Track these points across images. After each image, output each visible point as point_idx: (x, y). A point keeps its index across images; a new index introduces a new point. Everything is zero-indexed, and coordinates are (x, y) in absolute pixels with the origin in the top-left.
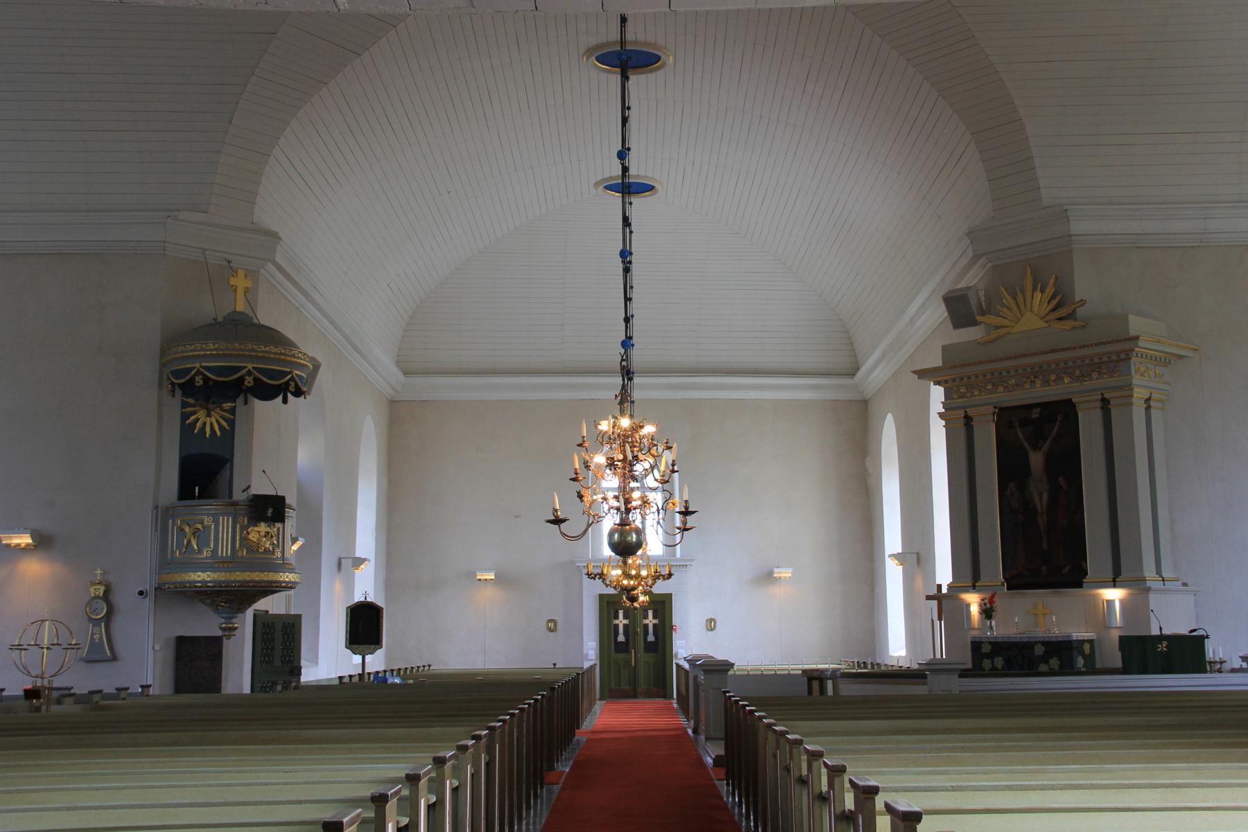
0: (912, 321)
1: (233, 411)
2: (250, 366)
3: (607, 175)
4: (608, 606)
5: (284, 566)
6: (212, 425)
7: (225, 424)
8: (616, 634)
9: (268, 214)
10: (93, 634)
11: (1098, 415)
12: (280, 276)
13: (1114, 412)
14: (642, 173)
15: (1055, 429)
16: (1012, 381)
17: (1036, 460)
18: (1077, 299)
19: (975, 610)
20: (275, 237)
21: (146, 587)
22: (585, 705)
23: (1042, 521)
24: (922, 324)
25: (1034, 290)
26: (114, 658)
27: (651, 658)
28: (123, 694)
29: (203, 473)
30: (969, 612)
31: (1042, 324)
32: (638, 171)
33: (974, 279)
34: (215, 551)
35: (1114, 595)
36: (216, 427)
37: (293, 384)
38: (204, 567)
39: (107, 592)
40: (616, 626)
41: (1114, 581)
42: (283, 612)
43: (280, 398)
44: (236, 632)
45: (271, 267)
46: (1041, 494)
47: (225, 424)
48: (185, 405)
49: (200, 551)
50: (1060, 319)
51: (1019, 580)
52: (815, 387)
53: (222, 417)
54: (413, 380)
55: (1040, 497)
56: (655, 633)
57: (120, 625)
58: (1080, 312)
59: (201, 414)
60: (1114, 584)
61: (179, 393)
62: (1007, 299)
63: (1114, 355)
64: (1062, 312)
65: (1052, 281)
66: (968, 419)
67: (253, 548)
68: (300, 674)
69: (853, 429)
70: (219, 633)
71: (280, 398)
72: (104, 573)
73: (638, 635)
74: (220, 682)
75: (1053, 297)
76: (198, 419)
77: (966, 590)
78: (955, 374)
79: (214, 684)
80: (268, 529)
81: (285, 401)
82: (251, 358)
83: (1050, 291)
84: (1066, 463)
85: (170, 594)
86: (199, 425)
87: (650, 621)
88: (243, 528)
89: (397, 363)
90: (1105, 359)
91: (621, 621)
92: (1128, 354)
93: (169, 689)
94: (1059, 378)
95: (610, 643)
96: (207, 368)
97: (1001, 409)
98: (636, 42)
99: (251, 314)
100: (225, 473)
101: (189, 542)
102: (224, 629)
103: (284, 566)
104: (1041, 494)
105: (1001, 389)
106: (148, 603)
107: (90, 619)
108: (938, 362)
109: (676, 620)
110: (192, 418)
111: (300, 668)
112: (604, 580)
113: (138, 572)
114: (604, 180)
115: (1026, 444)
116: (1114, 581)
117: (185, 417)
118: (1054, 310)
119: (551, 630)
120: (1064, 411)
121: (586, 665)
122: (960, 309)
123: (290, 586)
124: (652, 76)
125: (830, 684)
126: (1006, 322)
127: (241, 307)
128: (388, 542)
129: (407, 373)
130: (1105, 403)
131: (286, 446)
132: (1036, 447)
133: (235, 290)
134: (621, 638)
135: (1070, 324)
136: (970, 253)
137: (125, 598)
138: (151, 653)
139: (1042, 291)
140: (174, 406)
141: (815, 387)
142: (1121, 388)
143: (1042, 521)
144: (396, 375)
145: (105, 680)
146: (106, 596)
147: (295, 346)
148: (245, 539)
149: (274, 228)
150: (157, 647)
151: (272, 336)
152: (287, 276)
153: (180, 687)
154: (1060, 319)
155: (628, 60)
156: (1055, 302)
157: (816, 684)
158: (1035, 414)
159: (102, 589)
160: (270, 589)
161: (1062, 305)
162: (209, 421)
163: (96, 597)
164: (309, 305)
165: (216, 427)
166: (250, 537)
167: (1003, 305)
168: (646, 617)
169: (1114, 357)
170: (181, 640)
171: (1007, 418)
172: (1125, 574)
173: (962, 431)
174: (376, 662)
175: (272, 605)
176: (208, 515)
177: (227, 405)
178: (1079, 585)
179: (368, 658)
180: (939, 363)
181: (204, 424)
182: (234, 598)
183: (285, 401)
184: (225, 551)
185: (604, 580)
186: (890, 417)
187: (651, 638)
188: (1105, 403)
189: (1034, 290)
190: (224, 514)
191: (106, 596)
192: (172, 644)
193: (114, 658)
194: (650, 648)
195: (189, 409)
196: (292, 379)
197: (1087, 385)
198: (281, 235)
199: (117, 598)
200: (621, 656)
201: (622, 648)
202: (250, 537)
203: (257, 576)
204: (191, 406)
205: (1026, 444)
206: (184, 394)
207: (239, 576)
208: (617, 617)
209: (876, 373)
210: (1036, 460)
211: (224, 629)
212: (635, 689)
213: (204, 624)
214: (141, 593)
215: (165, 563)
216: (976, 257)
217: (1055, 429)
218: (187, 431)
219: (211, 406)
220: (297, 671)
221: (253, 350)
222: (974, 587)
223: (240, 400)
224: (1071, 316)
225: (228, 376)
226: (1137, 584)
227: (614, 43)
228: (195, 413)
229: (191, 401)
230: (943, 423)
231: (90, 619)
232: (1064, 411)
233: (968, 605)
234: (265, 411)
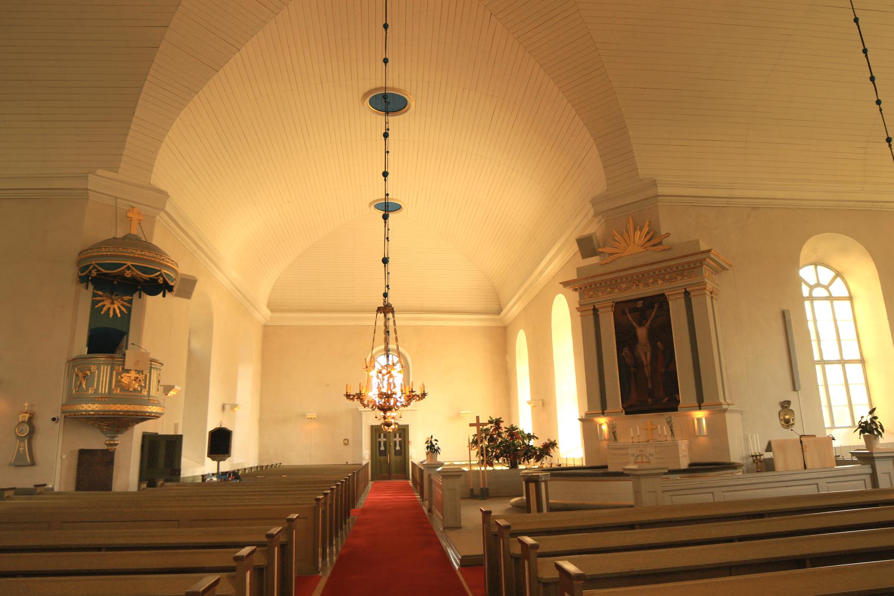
0: (541, 272)
1: (130, 302)
2: (129, 263)
3: (376, 198)
4: (376, 431)
5: (148, 401)
6: (114, 310)
7: (124, 310)
8: (395, 446)
9: (160, 178)
10: (19, 447)
11: (682, 302)
12: (178, 230)
13: (694, 301)
14: (396, 86)
15: (653, 314)
16: (623, 286)
17: (642, 333)
18: (663, 233)
19: (605, 428)
20: (165, 194)
21: (58, 414)
22: (361, 486)
23: (647, 371)
24: (560, 260)
25: (635, 230)
26: (33, 463)
27: (398, 458)
28: (39, 490)
29: (108, 340)
30: (601, 429)
31: (642, 249)
32: (394, 197)
33: (594, 229)
34: (97, 390)
35: (700, 414)
36: (118, 311)
37: (161, 279)
38: (93, 401)
39: (30, 419)
40: (380, 442)
41: (700, 406)
42: (172, 433)
43: (161, 294)
44: (117, 447)
45: (162, 214)
46: (646, 354)
47: (124, 310)
48: (95, 295)
49: (87, 390)
50: (654, 245)
51: (632, 407)
52: (481, 320)
53: (122, 305)
54: (277, 315)
55: (644, 352)
56: (400, 446)
57: (39, 442)
58: (665, 241)
59: (107, 303)
60: (700, 408)
61: (91, 287)
62: (618, 237)
63: (693, 264)
64: (652, 243)
65: (647, 223)
66: (595, 310)
67: (124, 388)
68: (179, 474)
69: (501, 340)
70: (105, 447)
71: (161, 294)
72: (31, 405)
73: (390, 444)
74: (111, 480)
75: (648, 233)
76: (104, 306)
77: (598, 415)
78: (586, 289)
79: (106, 484)
80: (137, 375)
81: (164, 296)
82: (129, 258)
83: (646, 229)
84: (662, 333)
85: (74, 420)
86: (105, 309)
87: (398, 439)
88: (118, 374)
89: (268, 306)
90: (686, 267)
91: (383, 439)
92: (701, 262)
93: (71, 487)
94: (655, 281)
95: (378, 452)
96: (99, 264)
97: (617, 303)
98: (393, 89)
99: (141, 236)
100: (124, 342)
101: (81, 383)
102: (108, 445)
103: (148, 401)
104: (646, 354)
105: (616, 291)
106: (58, 426)
107: (18, 437)
108: (574, 276)
109: (411, 439)
110: (100, 304)
111: (179, 471)
112: (362, 401)
113: (51, 406)
114: (374, 201)
115: (635, 324)
116: (700, 406)
117: (94, 303)
118: (649, 240)
119: (346, 444)
120: (660, 302)
121: (364, 463)
122: (586, 246)
123: (156, 416)
124: (401, 117)
125: (543, 485)
126: (618, 251)
127: (135, 231)
128: (261, 398)
129: (272, 311)
130: (687, 294)
131: (157, 321)
132: (641, 325)
133: (131, 221)
134: (382, 448)
135: (660, 247)
136: (592, 213)
137: (43, 422)
138: (59, 461)
139: (641, 230)
140: (87, 294)
141: (481, 320)
142: (698, 284)
143: (647, 371)
144: (269, 312)
145: (25, 479)
146: (30, 422)
147: (166, 254)
148: (118, 382)
149: (164, 188)
150: (64, 457)
151: (149, 247)
152: (207, 256)
153: (79, 487)
154: (654, 245)
155: (389, 103)
156: (648, 238)
157: (532, 486)
158: (640, 304)
159: (27, 416)
160: (143, 417)
161: (654, 239)
162: (114, 307)
163: (23, 422)
164: (198, 251)
165: (118, 311)
166: (123, 380)
167: (616, 241)
168: (395, 437)
169: (692, 265)
170: (82, 452)
171: (620, 309)
172: (706, 402)
173: (591, 318)
174: (226, 466)
175: (148, 427)
176: (94, 364)
177: (127, 298)
178: (676, 409)
179: (221, 463)
180: (575, 277)
181: (109, 309)
182: (119, 423)
183: (164, 296)
184: (104, 389)
185: (362, 401)
186: (249, 572)
187: (398, 448)
188: (687, 294)
189: (635, 230)
190: (104, 364)
191: (30, 422)
192: (77, 452)
193: (33, 463)
194: (397, 453)
195: (98, 298)
196: (161, 275)
197: (674, 284)
198: (170, 194)
199: (38, 423)
200: (383, 458)
201: (383, 453)
202: (123, 380)
203: (137, 408)
204: (101, 296)
205: (635, 324)
206: (96, 288)
207: (119, 407)
208: (380, 437)
209: (513, 310)
210: (642, 333)
211: (108, 445)
212: (390, 474)
213: (96, 441)
214: (54, 419)
215: (74, 397)
216: (596, 215)
217: (653, 314)
218: (95, 312)
219: (114, 297)
220: (178, 471)
221: (132, 253)
222: (603, 414)
223: (136, 295)
224: (660, 243)
225: (125, 280)
226: (718, 411)
227: (382, 199)
228: (103, 301)
229: (100, 293)
230: (579, 313)
231: (18, 437)
232: (660, 302)
233: (601, 425)
234: (153, 303)
